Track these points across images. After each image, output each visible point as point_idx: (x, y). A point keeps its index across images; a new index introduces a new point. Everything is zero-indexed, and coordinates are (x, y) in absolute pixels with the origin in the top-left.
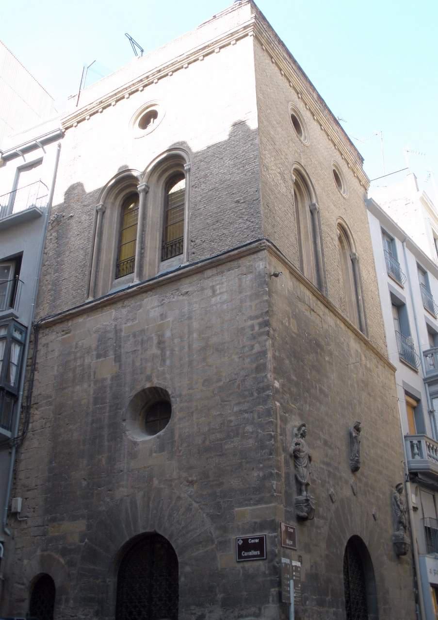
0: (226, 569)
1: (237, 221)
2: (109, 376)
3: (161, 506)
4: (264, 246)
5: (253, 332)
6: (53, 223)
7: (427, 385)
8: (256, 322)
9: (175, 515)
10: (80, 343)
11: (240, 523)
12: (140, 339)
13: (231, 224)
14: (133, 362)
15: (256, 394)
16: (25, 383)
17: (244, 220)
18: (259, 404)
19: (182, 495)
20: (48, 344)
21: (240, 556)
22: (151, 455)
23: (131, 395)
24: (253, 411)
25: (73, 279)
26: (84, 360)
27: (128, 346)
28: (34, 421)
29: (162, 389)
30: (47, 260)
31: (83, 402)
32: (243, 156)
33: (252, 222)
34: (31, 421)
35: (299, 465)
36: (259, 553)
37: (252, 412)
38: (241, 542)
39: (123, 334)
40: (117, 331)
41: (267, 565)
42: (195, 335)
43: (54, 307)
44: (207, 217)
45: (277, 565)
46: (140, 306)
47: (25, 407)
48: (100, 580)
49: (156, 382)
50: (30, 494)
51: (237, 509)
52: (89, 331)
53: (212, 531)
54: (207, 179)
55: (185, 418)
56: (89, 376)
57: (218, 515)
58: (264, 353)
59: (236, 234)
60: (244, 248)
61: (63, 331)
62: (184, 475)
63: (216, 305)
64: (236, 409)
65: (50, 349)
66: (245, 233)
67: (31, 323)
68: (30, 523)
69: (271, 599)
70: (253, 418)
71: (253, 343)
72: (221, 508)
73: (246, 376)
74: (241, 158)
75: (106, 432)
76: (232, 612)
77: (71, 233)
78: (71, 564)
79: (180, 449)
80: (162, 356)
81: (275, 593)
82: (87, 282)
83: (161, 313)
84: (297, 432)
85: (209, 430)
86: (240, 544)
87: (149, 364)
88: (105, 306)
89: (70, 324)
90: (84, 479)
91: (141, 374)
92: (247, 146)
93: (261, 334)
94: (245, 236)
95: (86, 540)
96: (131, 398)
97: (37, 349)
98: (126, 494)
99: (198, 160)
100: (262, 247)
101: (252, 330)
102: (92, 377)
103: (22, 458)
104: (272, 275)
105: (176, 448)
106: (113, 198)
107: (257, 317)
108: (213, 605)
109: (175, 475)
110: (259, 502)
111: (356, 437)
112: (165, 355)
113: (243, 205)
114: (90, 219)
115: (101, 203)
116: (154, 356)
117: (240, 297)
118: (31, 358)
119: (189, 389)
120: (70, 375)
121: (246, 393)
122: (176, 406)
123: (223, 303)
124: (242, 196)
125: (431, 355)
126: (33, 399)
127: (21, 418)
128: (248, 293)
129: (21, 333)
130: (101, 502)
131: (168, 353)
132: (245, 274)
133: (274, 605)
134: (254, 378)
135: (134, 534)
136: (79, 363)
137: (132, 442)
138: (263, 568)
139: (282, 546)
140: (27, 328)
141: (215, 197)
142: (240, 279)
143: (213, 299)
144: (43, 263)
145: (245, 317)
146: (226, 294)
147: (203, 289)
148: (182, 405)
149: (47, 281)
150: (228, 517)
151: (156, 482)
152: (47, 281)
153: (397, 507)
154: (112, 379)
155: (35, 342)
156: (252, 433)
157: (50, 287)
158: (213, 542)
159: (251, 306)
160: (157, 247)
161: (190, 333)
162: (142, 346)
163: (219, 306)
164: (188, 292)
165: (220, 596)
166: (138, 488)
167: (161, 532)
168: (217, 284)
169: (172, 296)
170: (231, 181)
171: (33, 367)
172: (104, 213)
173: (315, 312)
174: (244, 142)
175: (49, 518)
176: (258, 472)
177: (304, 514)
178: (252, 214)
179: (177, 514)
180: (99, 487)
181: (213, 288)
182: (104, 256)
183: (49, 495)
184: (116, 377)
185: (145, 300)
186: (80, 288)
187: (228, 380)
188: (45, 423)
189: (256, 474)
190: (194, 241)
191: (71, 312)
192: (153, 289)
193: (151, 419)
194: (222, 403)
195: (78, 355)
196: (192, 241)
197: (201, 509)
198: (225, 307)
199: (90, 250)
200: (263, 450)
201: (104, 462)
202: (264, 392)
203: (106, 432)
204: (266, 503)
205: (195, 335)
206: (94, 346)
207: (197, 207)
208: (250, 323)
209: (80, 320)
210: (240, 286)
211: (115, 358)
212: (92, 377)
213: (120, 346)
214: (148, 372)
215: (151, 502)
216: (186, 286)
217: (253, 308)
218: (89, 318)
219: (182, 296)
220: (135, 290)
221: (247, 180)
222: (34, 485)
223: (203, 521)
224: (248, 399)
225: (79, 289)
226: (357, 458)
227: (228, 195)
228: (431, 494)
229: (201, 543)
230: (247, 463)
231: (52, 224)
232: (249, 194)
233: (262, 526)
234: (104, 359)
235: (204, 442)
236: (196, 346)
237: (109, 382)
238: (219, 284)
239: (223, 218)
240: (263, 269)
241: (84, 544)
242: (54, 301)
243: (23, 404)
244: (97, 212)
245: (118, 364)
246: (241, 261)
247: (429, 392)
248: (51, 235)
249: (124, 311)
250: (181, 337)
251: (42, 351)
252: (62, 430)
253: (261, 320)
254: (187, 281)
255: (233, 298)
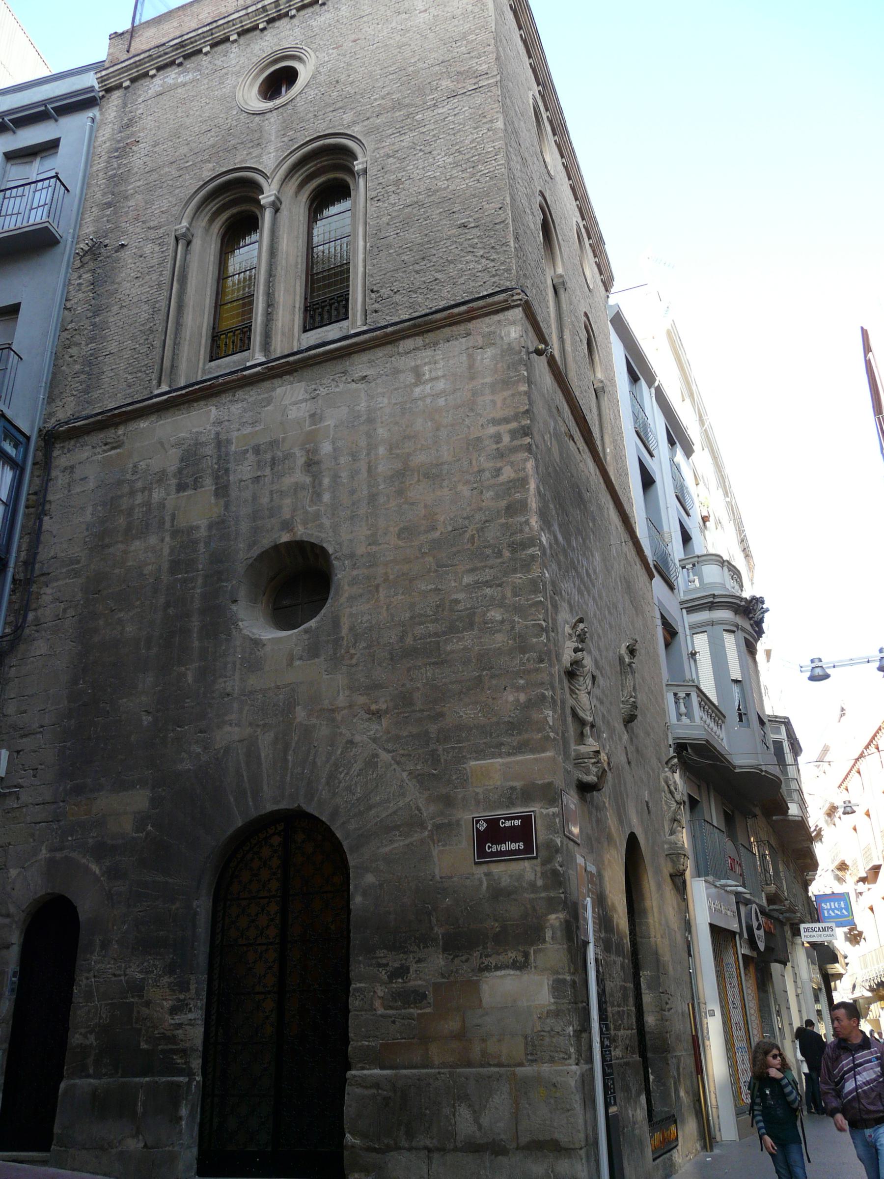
0: (451, 877)
1: (463, 259)
2: (203, 523)
3: (311, 758)
4: (517, 300)
5: (499, 446)
6: (84, 255)
7: (684, 611)
8: (503, 428)
9: (342, 775)
10: (143, 465)
11: (479, 790)
12: (268, 456)
13: (451, 262)
14: (255, 498)
15: (507, 554)
16: (21, 538)
17: (477, 257)
18: (515, 571)
19: (358, 738)
20: (72, 467)
21: (482, 853)
22: (290, 664)
23: (249, 556)
24: (503, 582)
25: (127, 354)
26: (150, 495)
27: (244, 470)
28: (40, 607)
29: (312, 545)
30: (72, 321)
31: (147, 570)
32: (471, 148)
33: (493, 260)
34: (34, 606)
35: (578, 689)
36: (522, 847)
37: (500, 585)
38: (483, 826)
39: (233, 448)
40: (220, 443)
41: (538, 869)
42: (381, 450)
43: (88, 403)
44: (402, 251)
45: (559, 868)
46: (269, 401)
47: (20, 580)
48: (178, 905)
49: (301, 532)
50: (26, 743)
51: (473, 763)
52: (162, 444)
53: (421, 805)
54: (401, 186)
55: (361, 596)
56: (162, 523)
57: (434, 775)
58: (522, 482)
59: (462, 280)
60: (481, 303)
61: (106, 444)
62: (362, 700)
63: (423, 398)
64: (466, 580)
65: (77, 476)
66: (479, 279)
67: (36, 429)
68: (25, 798)
69: (548, 934)
70: (504, 597)
71: (499, 465)
72: (439, 761)
73: (486, 521)
74: (469, 152)
75: (195, 623)
76: (467, 960)
77: (123, 275)
78: (114, 873)
79: (352, 651)
80: (314, 487)
81: (557, 924)
82: (158, 359)
83: (312, 412)
84: (570, 631)
85: (412, 618)
86: (482, 829)
87: (288, 501)
88: (196, 400)
89: (120, 432)
90: (146, 711)
91: (269, 517)
92: (482, 133)
93: (514, 450)
94: (480, 284)
95: (149, 828)
96: (251, 561)
97: (49, 475)
98: (236, 738)
99: (382, 155)
100: (514, 301)
101: (498, 443)
102: (168, 525)
103: (9, 676)
104: (532, 352)
105: (343, 651)
106: (207, 218)
107: (506, 420)
108: (424, 948)
109: (342, 700)
110: (521, 748)
111: (630, 665)
112: (320, 484)
113: (475, 231)
114: (162, 252)
115: (185, 223)
116: (297, 488)
117: (471, 386)
118: (35, 494)
119: (370, 545)
120: (122, 521)
121: (488, 551)
122: (342, 574)
123: (437, 395)
124: (471, 216)
125: (691, 566)
126: (37, 566)
127: (10, 602)
128: (488, 380)
129: (16, 446)
130: (184, 755)
131: (326, 481)
132: (481, 348)
133: (556, 947)
134: (502, 525)
135: (253, 814)
136: (139, 499)
137: (251, 639)
138: (529, 876)
139: (564, 835)
140: (28, 438)
141: (416, 218)
142: (470, 357)
143: (417, 391)
144: (63, 326)
145: (482, 421)
146: (443, 381)
147: (396, 372)
148: (355, 573)
149: (71, 357)
150: (454, 777)
151: (300, 714)
152: (71, 357)
153: (669, 796)
154: (210, 527)
155: (45, 465)
156: (502, 622)
157: (77, 367)
158: (422, 825)
159: (494, 402)
160: (297, 306)
161: (371, 447)
162: (272, 469)
163: (428, 401)
164: (366, 376)
165: (439, 931)
166: (265, 725)
167: (311, 809)
168: (425, 364)
169: (333, 384)
170: (448, 190)
171: (40, 508)
172: (189, 243)
173: (575, 443)
174: (475, 125)
175: (68, 787)
176: (516, 694)
177: (592, 778)
178: (493, 247)
179: (347, 773)
180: (178, 727)
181: (417, 372)
182: (190, 317)
183: (69, 744)
184: (218, 523)
185: (279, 390)
186: (144, 369)
187: (450, 529)
188: (65, 610)
189: (511, 698)
190: (378, 292)
191: (123, 409)
192: (296, 371)
193: (286, 603)
194: (440, 569)
195: (139, 485)
196: (372, 291)
197: (398, 763)
198: (441, 402)
199: (163, 304)
200: (524, 653)
201: (190, 679)
202: (523, 550)
203: (195, 623)
204: (533, 751)
205: (381, 450)
206: (172, 468)
207: (383, 235)
208: (492, 430)
209: (143, 424)
210: (471, 367)
211: (216, 489)
212: (168, 525)
213: (227, 470)
214: (286, 514)
215: (291, 752)
216: (360, 365)
217: (499, 404)
218: (162, 422)
219: (354, 384)
220: (259, 371)
221: (481, 190)
222: (36, 725)
223: (401, 787)
224: (490, 562)
225: (140, 371)
226: (632, 699)
227: (444, 214)
228: (696, 784)
229: (397, 827)
230: (493, 677)
231: (82, 257)
232: (486, 214)
233: (528, 794)
234: (194, 491)
235: (402, 639)
236: (383, 468)
237: (203, 532)
238: (429, 363)
239: (435, 252)
240: (516, 339)
241: (142, 835)
242: (86, 391)
243: (17, 577)
244: (177, 239)
245: (222, 502)
246: (471, 325)
247: (689, 623)
248: (80, 277)
249: (236, 409)
250: (354, 457)
251: (60, 479)
252: (101, 622)
253: (514, 425)
254: (365, 357)
255: (458, 387)
